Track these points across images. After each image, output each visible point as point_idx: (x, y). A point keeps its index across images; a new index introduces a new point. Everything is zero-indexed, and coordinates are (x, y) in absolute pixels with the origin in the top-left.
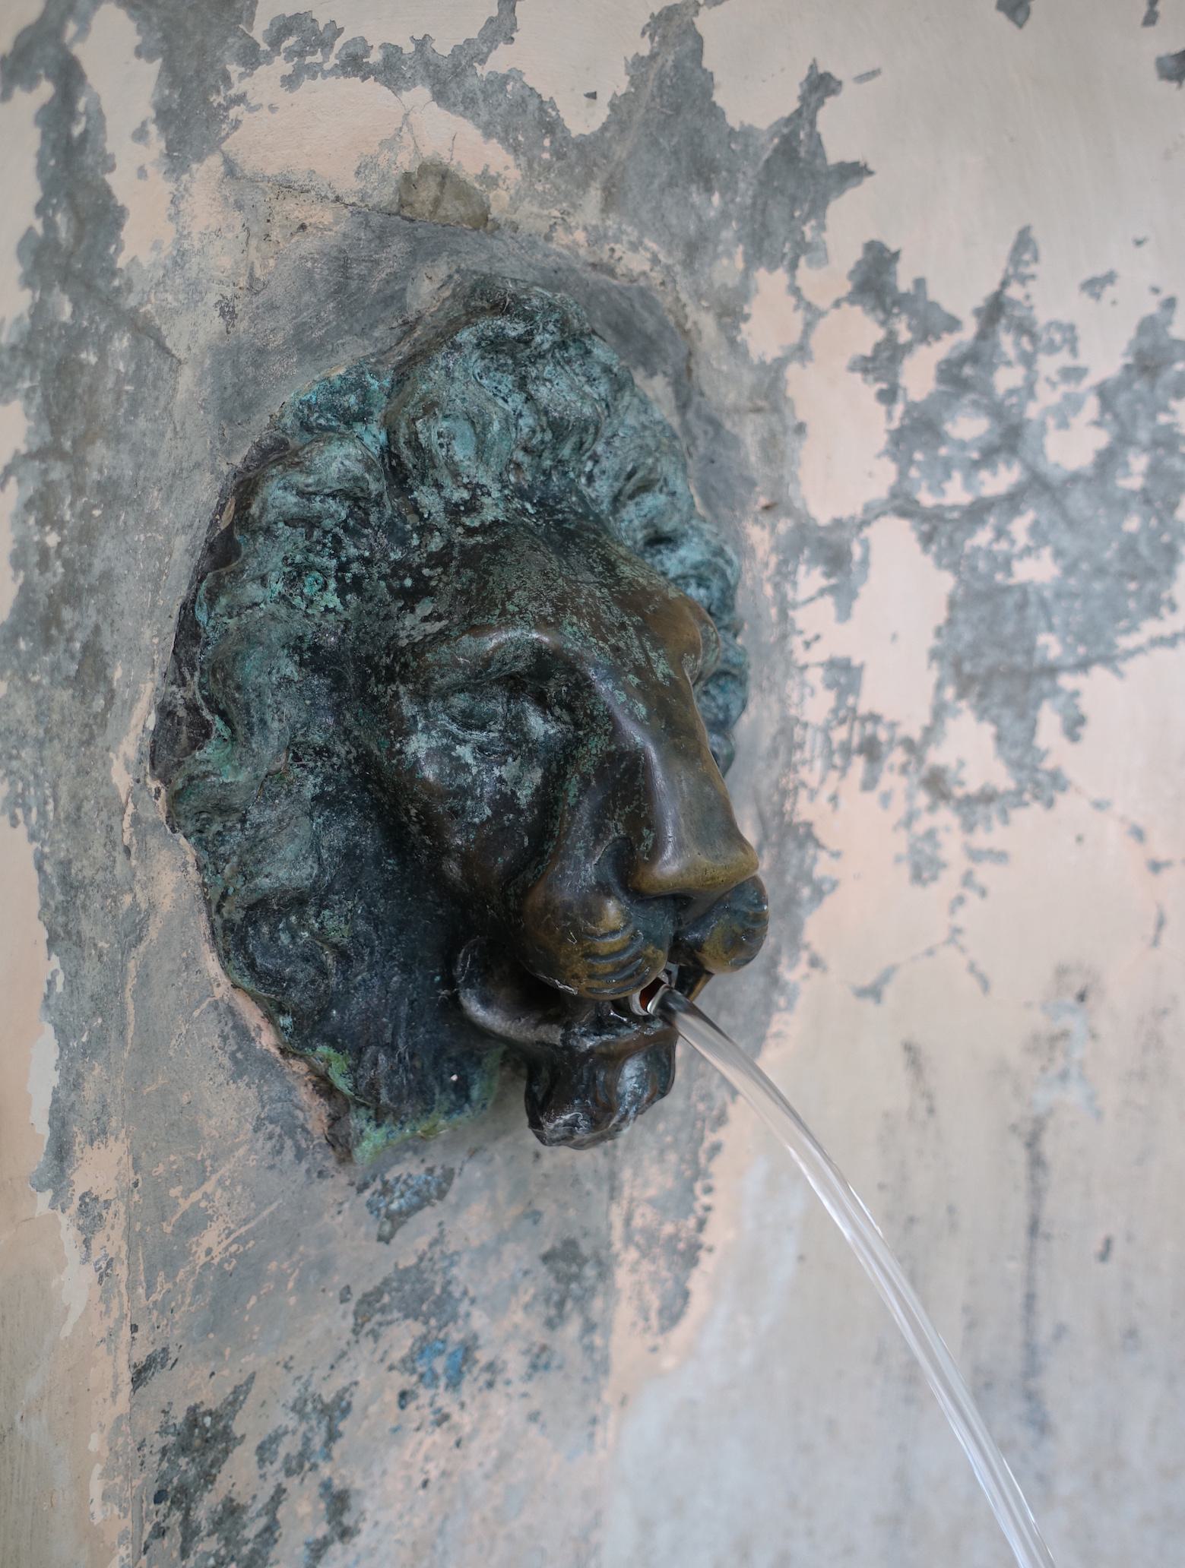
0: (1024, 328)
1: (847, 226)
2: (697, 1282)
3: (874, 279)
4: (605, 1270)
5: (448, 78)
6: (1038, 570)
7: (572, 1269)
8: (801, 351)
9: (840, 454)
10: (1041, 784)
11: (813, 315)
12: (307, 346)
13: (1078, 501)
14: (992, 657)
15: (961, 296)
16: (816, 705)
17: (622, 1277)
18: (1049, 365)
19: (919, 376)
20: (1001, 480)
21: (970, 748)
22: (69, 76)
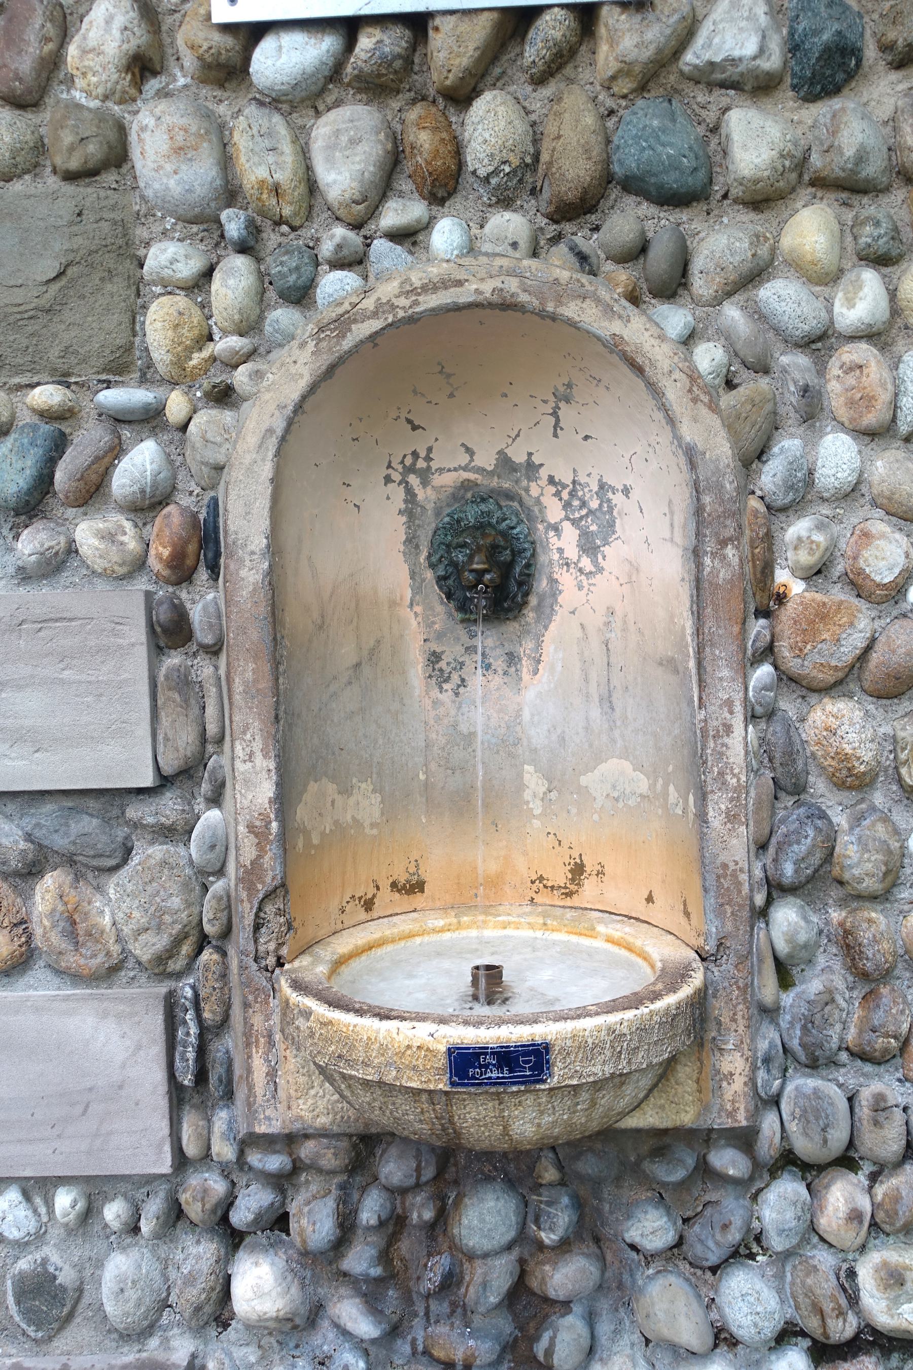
0: (580, 484)
1: (544, 473)
2: (540, 667)
3: (551, 480)
4: (520, 660)
5: (465, 469)
6: (594, 528)
7: (512, 658)
8: (542, 494)
9: (554, 511)
10: (600, 570)
11: (542, 488)
12: (448, 505)
13: (598, 514)
14: (588, 545)
15: (568, 481)
16: (556, 556)
17: (524, 662)
18: (586, 490)
19: (565, 495)
20: (584, 512)
21: (586, 563)
22: (407, 483)
